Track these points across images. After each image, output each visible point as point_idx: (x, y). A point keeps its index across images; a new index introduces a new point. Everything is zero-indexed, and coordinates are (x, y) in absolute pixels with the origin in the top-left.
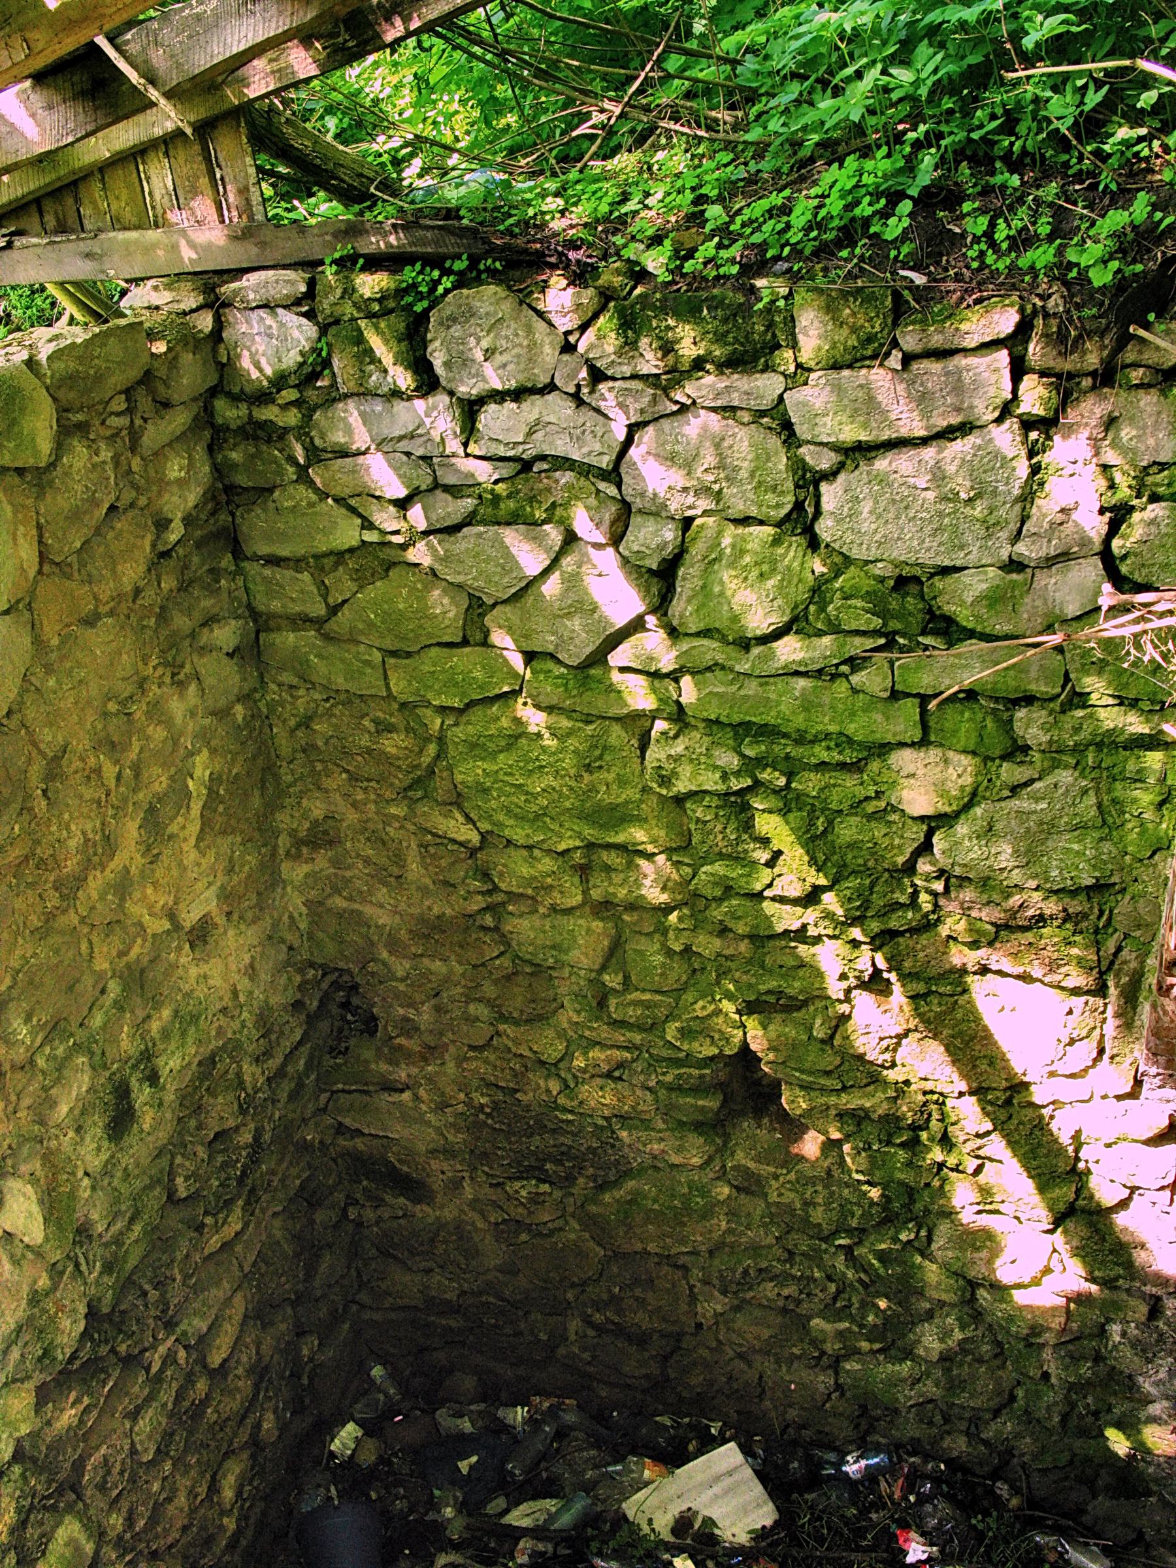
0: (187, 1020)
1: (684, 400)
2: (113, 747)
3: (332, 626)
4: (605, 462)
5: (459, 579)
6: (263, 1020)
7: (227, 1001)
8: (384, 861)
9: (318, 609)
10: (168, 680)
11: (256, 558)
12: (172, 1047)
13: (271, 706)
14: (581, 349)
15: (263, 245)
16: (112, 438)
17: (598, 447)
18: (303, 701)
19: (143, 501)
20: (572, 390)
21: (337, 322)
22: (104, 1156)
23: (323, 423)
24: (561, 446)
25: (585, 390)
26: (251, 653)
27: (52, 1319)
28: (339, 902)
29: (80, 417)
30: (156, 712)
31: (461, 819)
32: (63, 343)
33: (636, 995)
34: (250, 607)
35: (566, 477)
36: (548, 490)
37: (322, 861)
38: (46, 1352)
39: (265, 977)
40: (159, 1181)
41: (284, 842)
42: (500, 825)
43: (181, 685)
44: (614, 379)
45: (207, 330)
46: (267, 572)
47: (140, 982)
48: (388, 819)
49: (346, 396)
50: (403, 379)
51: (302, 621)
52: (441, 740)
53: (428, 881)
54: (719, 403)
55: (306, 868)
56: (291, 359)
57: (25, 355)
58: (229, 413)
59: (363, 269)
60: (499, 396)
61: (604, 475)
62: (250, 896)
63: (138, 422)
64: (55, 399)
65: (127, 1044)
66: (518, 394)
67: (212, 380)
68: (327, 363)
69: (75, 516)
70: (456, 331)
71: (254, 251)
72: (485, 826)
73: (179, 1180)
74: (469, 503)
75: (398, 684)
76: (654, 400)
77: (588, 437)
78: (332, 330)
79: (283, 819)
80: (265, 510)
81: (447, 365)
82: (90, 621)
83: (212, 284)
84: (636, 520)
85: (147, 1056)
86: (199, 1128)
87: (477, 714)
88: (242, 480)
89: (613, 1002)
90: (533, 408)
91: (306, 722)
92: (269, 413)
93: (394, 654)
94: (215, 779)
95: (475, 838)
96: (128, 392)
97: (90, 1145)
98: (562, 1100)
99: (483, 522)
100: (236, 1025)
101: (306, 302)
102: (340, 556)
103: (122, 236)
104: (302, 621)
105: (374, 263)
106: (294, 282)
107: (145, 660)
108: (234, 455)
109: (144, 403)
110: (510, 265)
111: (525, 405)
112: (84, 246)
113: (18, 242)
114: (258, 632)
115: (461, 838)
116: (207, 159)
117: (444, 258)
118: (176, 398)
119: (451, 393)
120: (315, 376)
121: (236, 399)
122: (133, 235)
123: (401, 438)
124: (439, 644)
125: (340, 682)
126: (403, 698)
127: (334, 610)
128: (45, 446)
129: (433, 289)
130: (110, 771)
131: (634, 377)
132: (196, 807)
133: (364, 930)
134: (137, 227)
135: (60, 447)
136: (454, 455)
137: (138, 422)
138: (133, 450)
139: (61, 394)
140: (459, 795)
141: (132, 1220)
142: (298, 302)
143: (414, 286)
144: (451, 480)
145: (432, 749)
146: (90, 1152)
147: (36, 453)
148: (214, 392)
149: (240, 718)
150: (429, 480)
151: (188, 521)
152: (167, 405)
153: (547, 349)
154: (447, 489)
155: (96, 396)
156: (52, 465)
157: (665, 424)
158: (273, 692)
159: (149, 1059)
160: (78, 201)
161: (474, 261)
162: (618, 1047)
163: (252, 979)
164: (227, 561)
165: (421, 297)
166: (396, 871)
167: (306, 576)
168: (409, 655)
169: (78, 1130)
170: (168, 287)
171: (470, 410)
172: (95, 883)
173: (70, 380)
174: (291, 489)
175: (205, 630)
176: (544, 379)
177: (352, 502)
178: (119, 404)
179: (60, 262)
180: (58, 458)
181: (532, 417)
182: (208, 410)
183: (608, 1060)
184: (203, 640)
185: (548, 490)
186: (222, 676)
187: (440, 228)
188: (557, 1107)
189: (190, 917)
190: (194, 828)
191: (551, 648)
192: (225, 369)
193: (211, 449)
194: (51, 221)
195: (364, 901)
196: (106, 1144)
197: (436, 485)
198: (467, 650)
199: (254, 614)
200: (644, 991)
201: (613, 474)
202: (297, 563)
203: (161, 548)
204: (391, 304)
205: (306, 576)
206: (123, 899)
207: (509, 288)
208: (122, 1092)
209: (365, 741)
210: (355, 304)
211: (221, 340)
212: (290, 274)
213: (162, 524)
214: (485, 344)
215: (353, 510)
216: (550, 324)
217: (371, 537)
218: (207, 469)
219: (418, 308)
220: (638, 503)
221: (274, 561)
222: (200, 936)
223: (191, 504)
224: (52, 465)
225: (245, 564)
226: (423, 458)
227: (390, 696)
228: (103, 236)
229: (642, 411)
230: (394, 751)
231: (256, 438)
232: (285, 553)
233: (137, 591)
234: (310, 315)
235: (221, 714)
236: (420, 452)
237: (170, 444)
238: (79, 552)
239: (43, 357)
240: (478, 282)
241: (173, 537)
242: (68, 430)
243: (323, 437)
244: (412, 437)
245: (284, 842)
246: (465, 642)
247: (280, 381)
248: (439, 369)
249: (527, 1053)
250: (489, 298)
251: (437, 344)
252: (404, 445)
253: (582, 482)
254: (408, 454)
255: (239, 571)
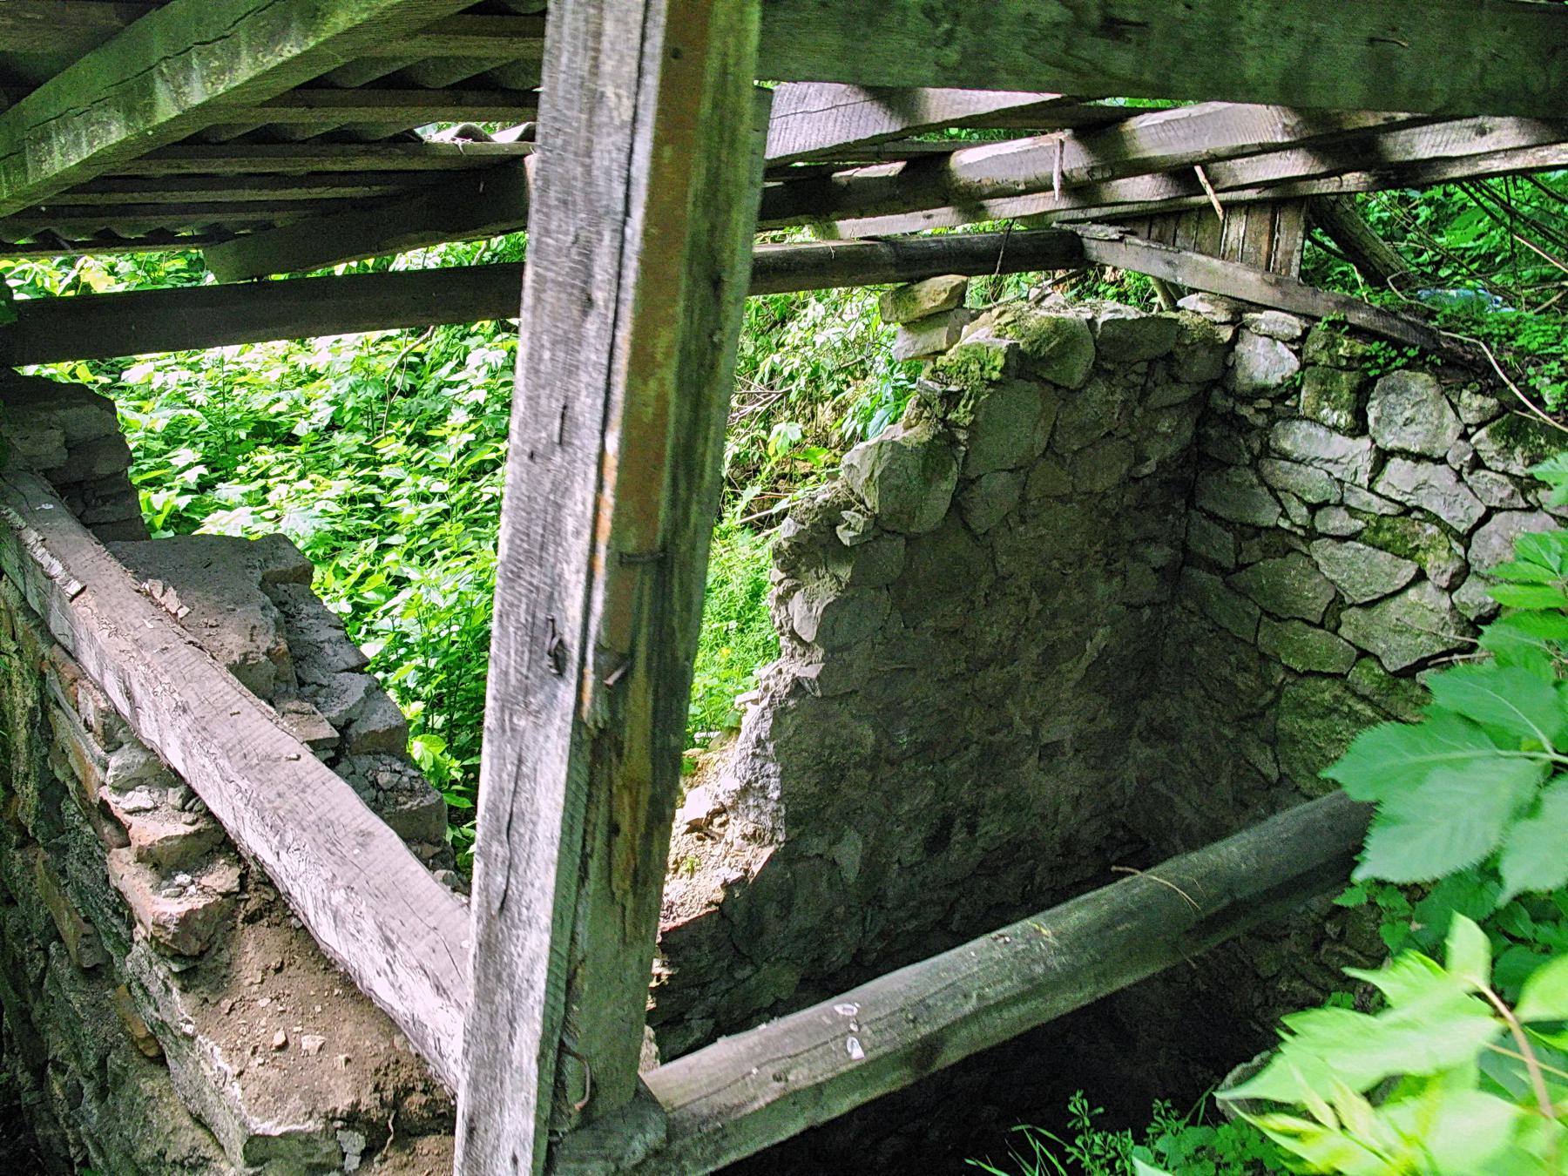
0: (1014, 805)
1: (1533, 501)
2: (1044, 589)
3: (1234, 578)
4: (1463, 528)
5: (1334, 577)
6: (1068, 845)
7: (1049, 812)
8: (1203, 767)
9: (1228, 562)
10: (1102, 563)
11: (1202, 509)
12: (994, 817)
13: (1172, 621)
14: (1473, 440)
15: (1285, 294)
16: (1127, 389)
17: (1461, 516)
18: (1195, 625)
19: (1134, 438)
20: (1457, 467)
21: (1315, 364)
22: (916, 858)
23: (1280, 431)
24: (1434, 506)
25: (1465, 470)
26: (1172, 575)
27: (833, 940)
28: (1159, 786)
29: (1110, 366)
30: (1085, 585)
31: (1270, 757)
32: (1119, 316)
33: (1345, 949)
34: (1184, 542)
35: (1432, 530)
36: (1417, 534)
37: (1161, 752)
38: (819, 958)
39: (1085, 813)
40: (943, 904)
41: (1140, 724)
42: (1296, 773)
43: (1111, 575)
44: (1489, 469)
45: (1226, 340)
46: (1205, 523)
47: (991, 757)
48: (1220, 737)
49: (1302, 418)
50: (1344, 418)
51: (1215, 567)
52: (1279, 690)
53: (1230, 797)
54: (1558, 513)
55: (1149, 751)
56: (1274, 380)
57: (1089, 316)
58: (1219, 401)
59: (1346, 333)
60: (1405, 454)
61: (1459, 537)
62: (1101, 749)
63: (1150, 384)
64: (1097, 350)
65: (965, 793)
66: (1419, 458)
67: (1216, 375)
68: (1298, 391)
69: (1081, 429)
70: (1392, 398)
71: (1279, 296)
72: (1285, 769)
73: (957, 916)
74: (1360, 524)
75: (1263, 638)
76: (1513, 495)
77: (1457, 505)
78: (1309, 369)
79: (1146, 707)
80: (1220, 476)
81: (1377, 420)
82: (1063, 499)
83: (1240, 311)
84: (1471, 579)
85: (975, 811)
86: (988, 890)
87: (1311, 682)
88: (1212, 451)
89: (1325, 947)
90: (1425, 470)
91: (1191, 643)
92: (1247, 411)
93: (1269, 615)
94: (1104, 653)
95: (1275, 776)
96: (1151, 362)
97: (908, 844)
98: (1259, 1013)
99: (1364, 542)
100: (1048, 834)
101: (1298, 344)
102: (1258, 530)
103: (1196, 257)
104: (1215, 567)
105: (1356, 331)
106: (1295, 326)
107: (1092, 544)
108: (1212, 432)
109: (1160, 373)
110: (1449, 364)
111: (1421, 467)
112: (1167, 256)
113: (1130, 239)
114: (1183, 564)
115: (1265, 771)
116: (1273, 224)
117: (1405, 344)
118: (1185, 378)
119: (1374, 441)
120: (1286, 396)
121: (1228, 393)
122: (1203, 259)
123: (1329, 461)
124: (1303, 620)
125: (1225, 622)
126: (1263, 649)
127: (1241, 567)
128: (1079, 377)
129: (1387, 364)
130: (1035, 605)
131: (1504, 473)
132: (1084, 663)
133: (1170, 815)
134: (1211, 255)
135: (1089, 380)
136: (1360, 486)
137: (1150, 384)
138: (1140, 402)
139: (1104, 349)
140: (1276, 738)
141: (912, 916)
142: (1292, 341)
143: (1376, 357)
144: (1353, 503)
145: (1270, 695)
146: (909, 847)
147: (1071, 379)
148: (1214, 383)
149: (1145, 618)
150: (1338, 498)
151: (1161, 464)
152: (1176, 380)
153: (1449, 432)
154: (1349, 508)
155: (1127, 357)
156: (1080, 390)
157: (1516, 515)
158: (1177, 612)
159: (976, 813)
160: (1177, 224)
161: (1423, 353)
162: (1317, 988)
163: (1074, 808)
164: (1180, 504)
165: (1378, 366)
166: (1209, 778)
167: (1230, 536)
168: (1280, 620)
169: (909, 829)
170: (1211, 302)
171: (1382, 457)
172: (993, 673)
173: (1114, 340)
174: (1242, 470)
175: (1144, 545)
176: (1439, 453)
177: (1281, 495)
178: (1142, 367)
179: (1149, 261)
180: (1085, 387)
181: (1423, 478)
182: (1207, 394)
183: (1305, 994)
184: (1140, 549)
185: (1417, 534)
186: (1146, 585)
187: (1408, 322)
188: (1253, 1017)
189: (1048, 736)
190: (1077, 676)
191: (1379, 653)
192: (1228, 370)
193: (1197, 425)
194: (1155, 232)
195: (1179, 793)
196: (920, 850)
197: (1341, 504)
198: (1321, 631)
199: (1185, 549)
200: (1351, 947)
201: (1466, 539)
202: (1227, 524)
203: (1133, 473)
204: (1355, 365)
205: (1230, 536)
206: (1006, 696)
207: (1438, 381)
208: (947, 822)
209: (1226, 671)
210: (1330, 356)
211: (1233, 350)
212: (1295, 321)
213: (1141, 459)
214: (1407, 414)
215: (1279, 501)
216: (1458, 415)
217: (1285, 524)
218: (1189, 434)
219: (1372, 373)
220: (1475, 567)
221: (1212, 516)
222: (1050, 752)
223: (1168, 453)
224: (1080, 390)
225: (1192, 511)
226: (1339, 480)
227: (1255, 645)
228: (1184, 253)
229: (1501, 500)
230: (1243, 687)
231: (1232, 426)
232: (1222, 514)
233: (1104, 496)
234: (1298, 353)
235: (1134, 608)
236: (1337, 475)
237: (1168, 407)
238: (1075, 453)
239: (1100, 321)
240: (1422, 369)
241: (1146, 471)
242: (1098, 371)
243: (1277, 440)
244: (1336, 463)
245: (1140, 724)
246: (1321, 626)
247: (1262, 391)
248: (1371, 421)
249: (1247, 962)
250: (1420, 382)
251: (1375, 403)
252: (1328, 466)
253: (1442, 537)
254: (1330, 474)
255: (1187, 513)
